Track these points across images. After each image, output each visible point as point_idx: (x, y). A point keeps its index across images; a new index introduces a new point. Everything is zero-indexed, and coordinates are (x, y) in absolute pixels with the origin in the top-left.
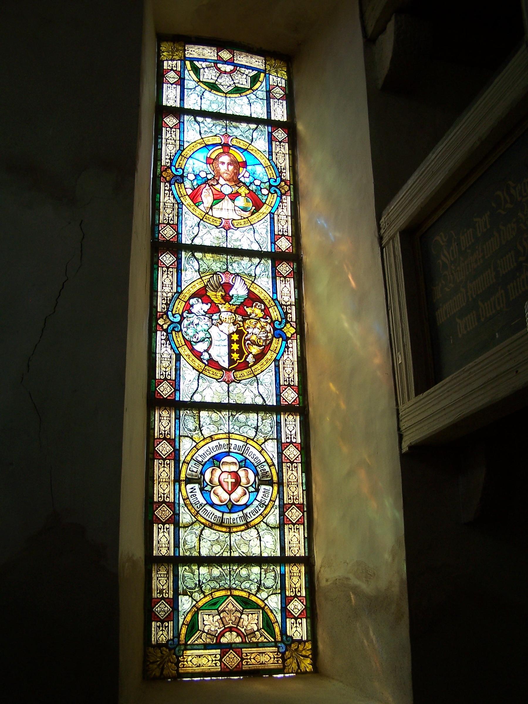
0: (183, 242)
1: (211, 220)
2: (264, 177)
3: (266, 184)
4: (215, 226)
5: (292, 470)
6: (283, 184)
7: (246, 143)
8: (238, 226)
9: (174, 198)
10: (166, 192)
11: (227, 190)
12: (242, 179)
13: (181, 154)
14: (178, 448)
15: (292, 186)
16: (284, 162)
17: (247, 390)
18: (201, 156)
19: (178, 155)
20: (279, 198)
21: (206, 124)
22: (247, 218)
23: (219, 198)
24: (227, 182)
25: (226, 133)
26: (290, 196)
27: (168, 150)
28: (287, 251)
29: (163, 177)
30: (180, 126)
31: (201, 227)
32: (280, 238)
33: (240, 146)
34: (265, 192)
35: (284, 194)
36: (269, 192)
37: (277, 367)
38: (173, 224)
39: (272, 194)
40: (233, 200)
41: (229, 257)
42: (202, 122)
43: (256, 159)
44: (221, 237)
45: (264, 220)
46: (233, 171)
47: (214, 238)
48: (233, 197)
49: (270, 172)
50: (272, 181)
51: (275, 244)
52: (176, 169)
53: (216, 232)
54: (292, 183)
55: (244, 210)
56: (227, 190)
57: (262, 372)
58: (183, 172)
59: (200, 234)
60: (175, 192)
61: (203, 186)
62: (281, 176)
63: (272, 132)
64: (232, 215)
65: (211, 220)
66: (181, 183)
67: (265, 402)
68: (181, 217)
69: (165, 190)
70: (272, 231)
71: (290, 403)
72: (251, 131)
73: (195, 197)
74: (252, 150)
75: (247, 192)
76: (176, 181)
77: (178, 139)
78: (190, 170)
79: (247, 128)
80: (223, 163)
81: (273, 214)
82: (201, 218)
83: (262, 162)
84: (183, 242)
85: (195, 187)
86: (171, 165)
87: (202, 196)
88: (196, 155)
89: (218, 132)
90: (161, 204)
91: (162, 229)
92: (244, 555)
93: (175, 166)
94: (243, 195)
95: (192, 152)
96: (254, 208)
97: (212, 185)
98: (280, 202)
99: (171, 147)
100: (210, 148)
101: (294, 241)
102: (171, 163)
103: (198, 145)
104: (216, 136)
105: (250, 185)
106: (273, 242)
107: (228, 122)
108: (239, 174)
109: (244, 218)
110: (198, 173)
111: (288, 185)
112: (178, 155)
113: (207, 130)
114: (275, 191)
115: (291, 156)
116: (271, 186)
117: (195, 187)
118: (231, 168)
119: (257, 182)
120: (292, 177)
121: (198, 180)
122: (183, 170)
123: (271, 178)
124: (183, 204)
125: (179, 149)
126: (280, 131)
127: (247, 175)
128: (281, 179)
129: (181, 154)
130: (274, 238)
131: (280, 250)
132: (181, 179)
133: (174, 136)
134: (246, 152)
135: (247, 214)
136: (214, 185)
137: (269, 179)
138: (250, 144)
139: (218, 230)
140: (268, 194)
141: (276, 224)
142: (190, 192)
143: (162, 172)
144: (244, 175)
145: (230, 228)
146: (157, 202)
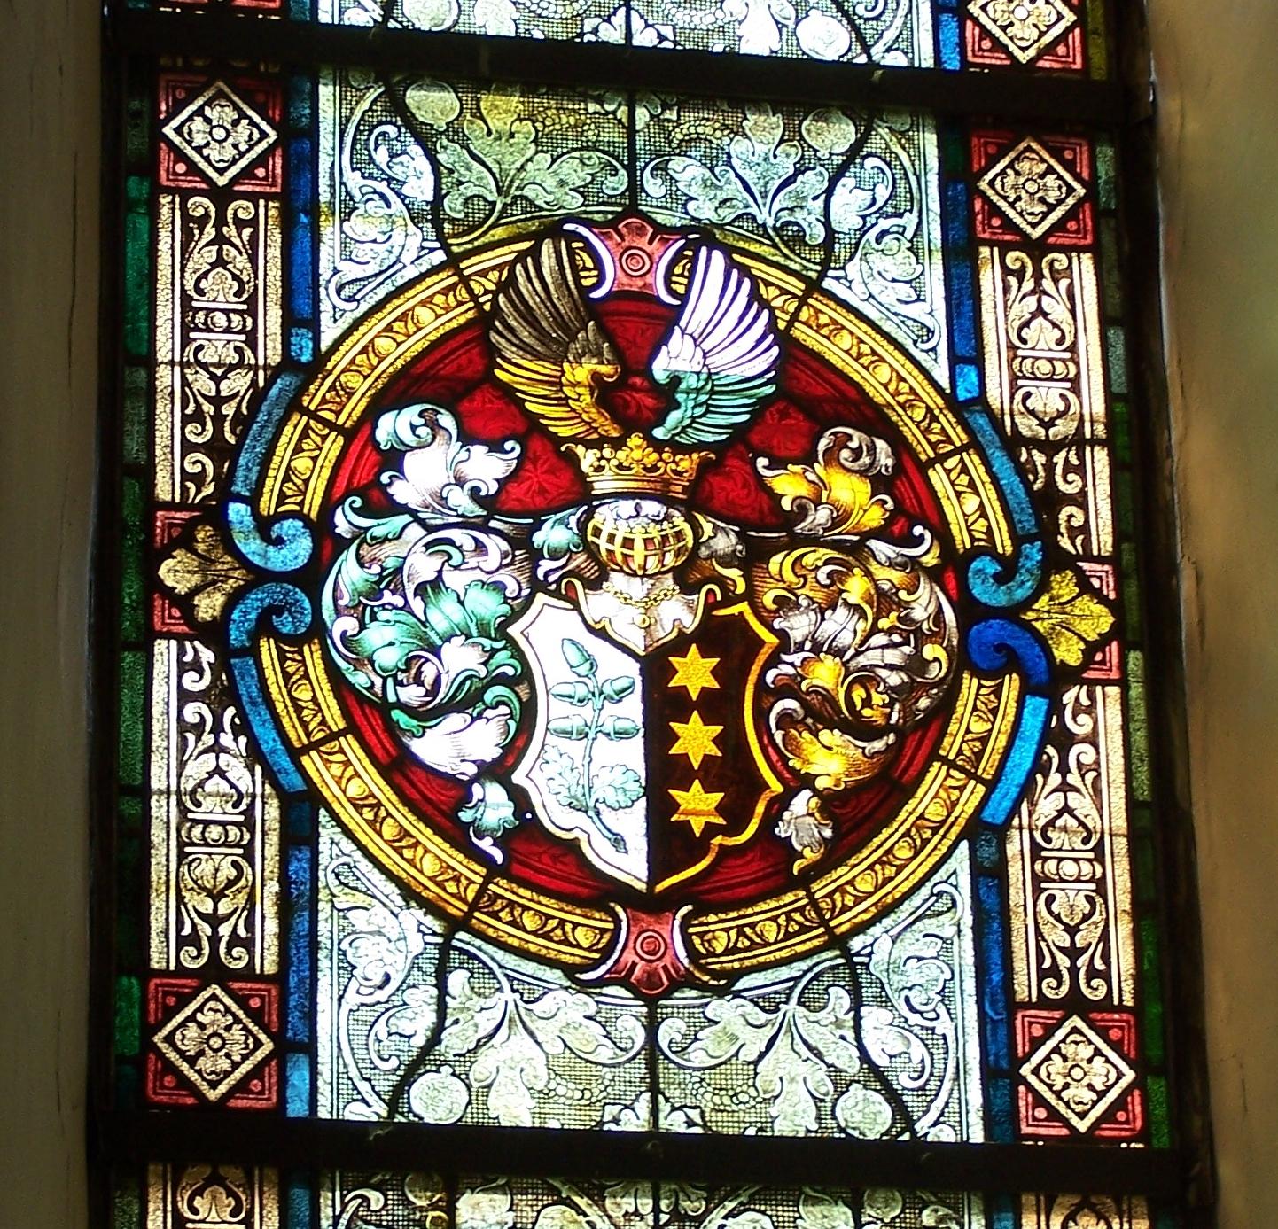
0: (324, 18)
20: (1037, 705)
41: (642, 115)
45: (925, 891)
51: (963, 16)
62: (1047, 532)
67: (866, 49)
71: (1023, 57)
84: (324, 18)
90: (163, 371)
131: (999, 60)
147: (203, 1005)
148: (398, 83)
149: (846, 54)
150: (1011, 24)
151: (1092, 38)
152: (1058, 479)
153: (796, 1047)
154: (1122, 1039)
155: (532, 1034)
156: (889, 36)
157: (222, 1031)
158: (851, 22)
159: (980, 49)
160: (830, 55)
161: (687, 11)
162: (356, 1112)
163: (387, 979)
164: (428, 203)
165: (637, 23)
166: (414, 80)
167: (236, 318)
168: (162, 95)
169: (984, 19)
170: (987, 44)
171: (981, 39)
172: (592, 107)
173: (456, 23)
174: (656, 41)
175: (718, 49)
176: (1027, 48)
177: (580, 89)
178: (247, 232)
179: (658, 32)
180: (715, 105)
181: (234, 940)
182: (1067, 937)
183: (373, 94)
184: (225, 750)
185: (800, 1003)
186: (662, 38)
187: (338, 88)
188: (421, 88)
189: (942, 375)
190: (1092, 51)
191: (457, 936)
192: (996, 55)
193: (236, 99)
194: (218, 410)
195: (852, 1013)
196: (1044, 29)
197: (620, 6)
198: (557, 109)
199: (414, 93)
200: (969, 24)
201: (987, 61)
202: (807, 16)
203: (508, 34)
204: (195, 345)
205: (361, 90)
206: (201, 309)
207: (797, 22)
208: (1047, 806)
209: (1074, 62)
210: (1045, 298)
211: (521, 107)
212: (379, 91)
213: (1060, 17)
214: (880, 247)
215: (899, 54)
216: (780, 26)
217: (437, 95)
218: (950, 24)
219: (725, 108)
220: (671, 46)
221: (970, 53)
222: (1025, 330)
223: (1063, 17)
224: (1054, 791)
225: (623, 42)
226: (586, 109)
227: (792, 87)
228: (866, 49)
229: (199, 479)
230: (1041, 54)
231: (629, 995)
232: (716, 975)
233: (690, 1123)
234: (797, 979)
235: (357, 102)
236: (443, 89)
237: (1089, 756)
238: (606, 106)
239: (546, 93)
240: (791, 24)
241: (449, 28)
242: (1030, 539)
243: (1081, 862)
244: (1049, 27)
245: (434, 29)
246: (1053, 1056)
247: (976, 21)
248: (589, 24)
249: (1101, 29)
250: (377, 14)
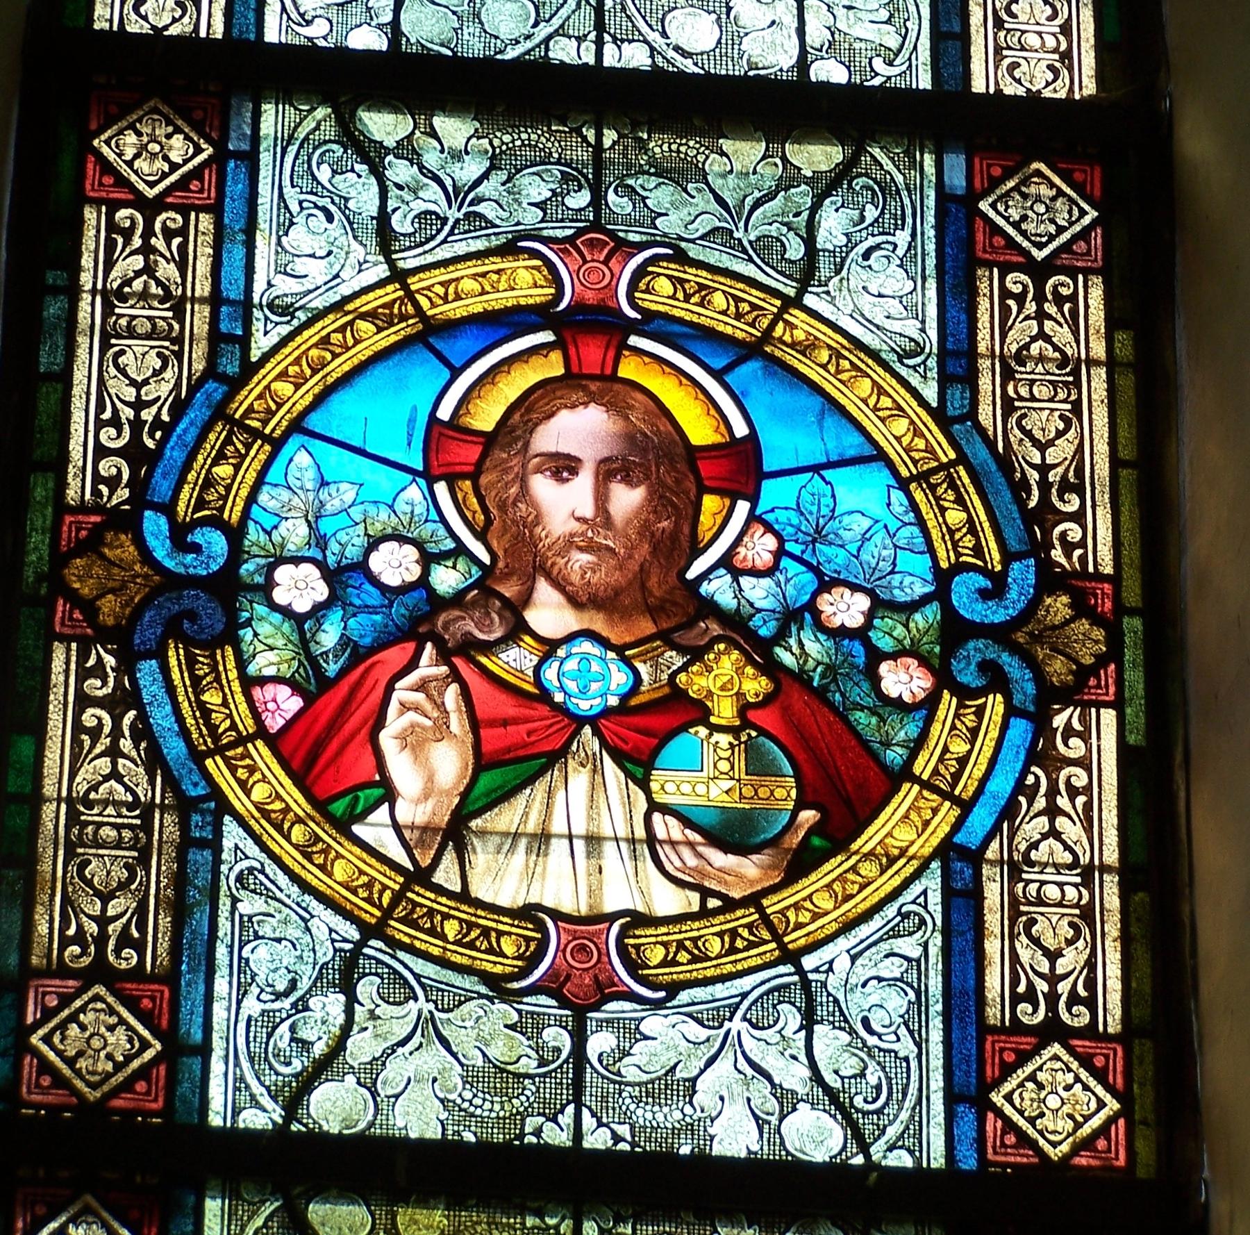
0: (215, 1120)
1: (451, 929)
2: (907, 561)
3: (919, 620)
4: (487, 978)
5: (1044, 469)
6: (1059, 606)
7: (755, 296)
8: (667, 975)
9: (154, 760)
10: (89, 717)
11: (593, 680)
12: (720, 589)
13: (220, 413)
14: (197, 1036)
15: (1133, 625)
16: (1072, 433)
17: (728, 1055)
18: (390, 411)
19: (196, 414)
20: (1020, 730)
21: (432, 159)
22: (754, 900)
23: (517, 749)
24: (597, 623)
25: (596, 226)
26: (1118, 704)
27: (114, 382)
28: (1082, 1161)
29: (74, 598)
30: (221, 193)
31: (366, 989)
32: (1024, 1057)
33: (706, 318)
34: (902, 681)
35: (1068, 695)
36: (943, 678)
37: (963, 901)
38: (137, 973)
39: (964, 693)
40: (638, 764)
41: (609, 137)
42: (407, 150)
43: (831, 421)
44: (529, 1065)
45: (891, 911)
46: (645, 529)
47: (470, 1078)
48: (641, 733)
49: (955, 517)
50: (964, 591)
51: (983, 1106)
52: (180, 537)
53: (486, 1030)
54: (1132, 594)
55: (731, 833)
56: (593, 680)
57: (848, 926)
58: (236, 553)
59: (361, 1048)
60: (161, 718)
61: (396, 656)
62: (1038, 550)
63: (972, 197)
64: (624, 886)
65: (451, 929)
66: (212, 645)
67: (864, 1148)
68: (200, 919)
69: (84, 701)
70: (963, 998)
71: (1054, 1154)
72: (802, 196)
73: (330, 758)
74: (806, 348)
75: (755, 686)
76: (173, 629)
77: (203, 288)
78: (295, 534)
79: (770, 173)
80: (563, 466)
81: (975, 857)
82: (371, 915)
83: (891, 434)
84: (215, 1120)
85: (332, 669)
86: (141, 497)
87: (387, 739)
88: (342, 416)
89: (531, 217)
90: (48, 811)
91: (48, 1014)
92: (689, 66)
93: (168, 510)
94: (725, 711)
95: (313, 386)
96: (808, 816)
97: (470, 648)
98: (1033, 757)
99: (140, 357)
100: (457, 349)
101: (1145, 1070)
102: (139, 487)
103: (365, 327)
104: (509, 249)
105: (780, 636)
106: (969, 1093)
107: (609, 137)
108: (697, 551)
109: (730, 905)
110: (353, 553)
111: (1097, 620)
112: (196, 414)
113: (442, 207)
114: (989, 668)
115: (1127, 382)
116: (955, 630)
117: (332, 669)
118: (627, 499)
119: (847, 609)
120: (1132, 553)
121: (351, 610)
122: (235, 535)
123: (959, 568)
124: (225, 807)
125: (211, 372)
126: (1046, 182)
127: (761, 548)
128: (1045, 567)
129: (220, 413)
130: (980, 1052)
131: (1024, 1158)
132: (212, 608)
133: (167, 270)
134: (752, 367)
135: (745, 871)
136: (488, 648)
137: (943, 579)
138: (791, 303)
139: (504, 1012)
140: (930, 703)
141: (992, 947)
142: (284, 705)
143: (60, 560)
144: (738, 558)
145: (606, 991)
146: (18, 798)
147: (87, 1003)
148: (299, 1196)
149: (840, 1153)
150: (1042, 1115)
151: (1140, 1130)
152: (1055, 499)
153: (739, 1066)
154: (1085, 181)
155: (447, 1047)
156: (892, 1132)
157: (108, 1049)
158: (847, 1116)
159: (1003, 1145)
160: (819, 1156)
161: (648, 1108)
162: (253, 1120)
163: (293, 985)
164: (373, 218)
165: (588, 1121)
166: (320, 1192)
167: (127, 834)
168: (19, 1210)
169: (1008, 1110)
170: (1011, 1139)
171: (1004, 1133)
172: (530, 1222)
173: (372, 1124)
174: (610, 1143)
175: (685, 1150)
176: (1060, 1143)
177: (518, 1201)
178: (176, 241)
179: (613, 1132)
180: (678, 1216)
182: (1038, 454)
183: (268, 1209)
184: (155, 250)
185: (744, 1019)
186: (617, 1138)
187: (281, 107)
188: (325, 1201)
189: (930, 393)
190: (1139, 1145)
191: (370, 943)
192: (1022, 1151)
193: (105, 1215)
194: (137, 415)
195: (804, 1032)
196: (1080, 1119)
197: (569, 1103)
198: (489, 1224)
199: (317, 1207)
200: (990, 1116)
201: (1012, 1159)
202: (794, 1109)
203: (434, 1137)
205: (254, 1204)
206: (124, 315)
207: (782, 1118)
208: (1034, 827)
209: (1117, 1159)
211: (446, 1222)
212: (277, 1204)
213: (1101, 1105)
214: (866, 263)
215: (903, 1153)
216: (760, 1123)
217: (344, 1208)
218: (967, 1117)
219: (692, 1219)
220: (628, 1148)
221: (990, 1150)
223: (1105, 1105)
225: (569, 1144)
226: (523, 1224)
227: (777, 106)
228: (864, 1148)
229: (113, 483)
230: (1076, 1150)
231: (554, 1003)
232: (654, 987)
233: (617, 1138)
234: (744, 995)
235: (250, 1219)
236: (353, 1202)
237: (1080, 779)
238: (547, 1219)
239: (477, 1205)
240: (774, 1120)
241: (363, 1131)
242: (1019, 557)
244: (1087, 1118)
245: (345, 1132)
247: (999, 1113)
248: (531, 1123)
249: (1151, 1117)
250: (277, 1114)
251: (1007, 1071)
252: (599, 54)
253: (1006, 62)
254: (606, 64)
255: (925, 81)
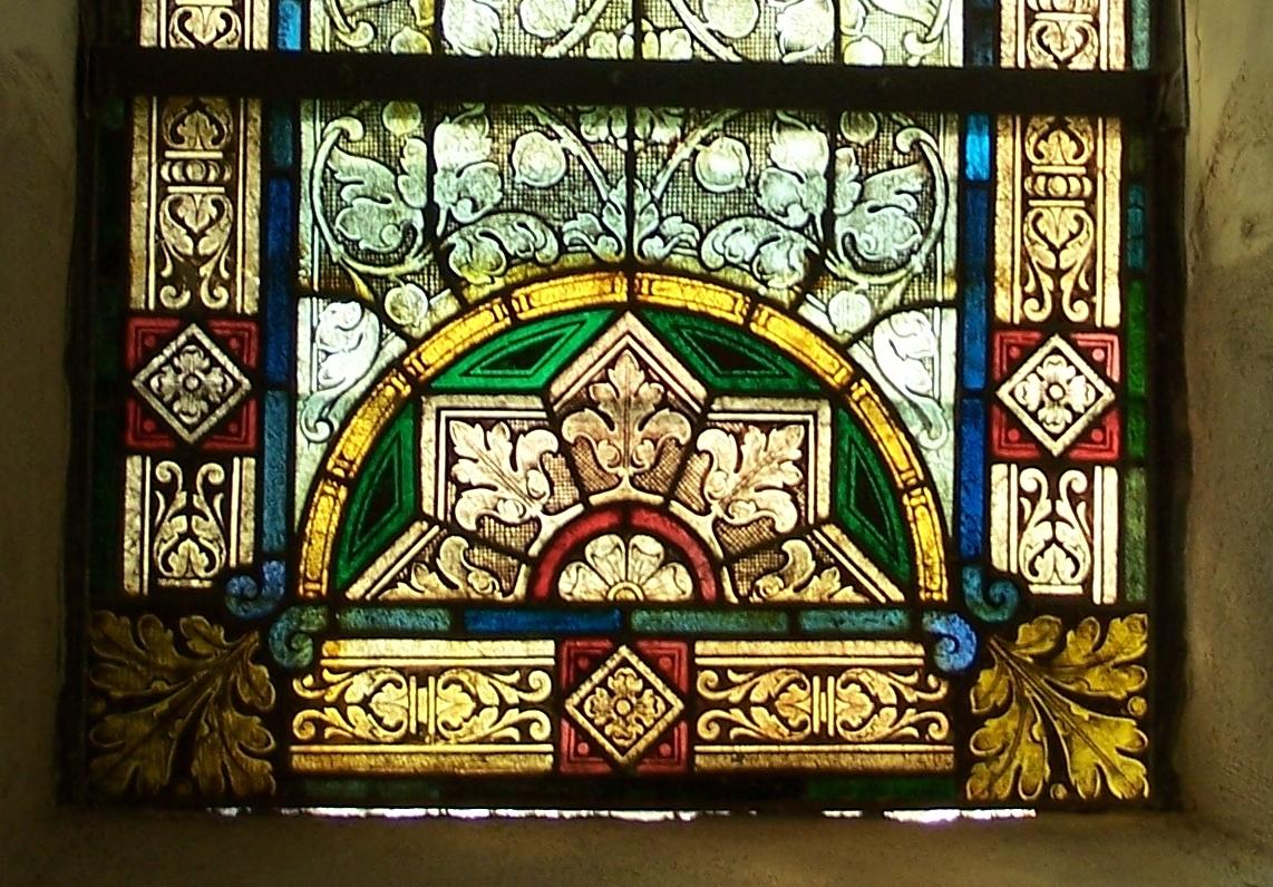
92: (726, 54)
181: (523, 686)
204: (180, 11)
210: (753, 698)
222: (459, 688)
224: (501, 697)
243: (1070, 179)
246: (641, 682)
251: (1015, 366)
252: (638, 49)
253: (1031, 215)
254: (645, 56)
255: (958, 61)
